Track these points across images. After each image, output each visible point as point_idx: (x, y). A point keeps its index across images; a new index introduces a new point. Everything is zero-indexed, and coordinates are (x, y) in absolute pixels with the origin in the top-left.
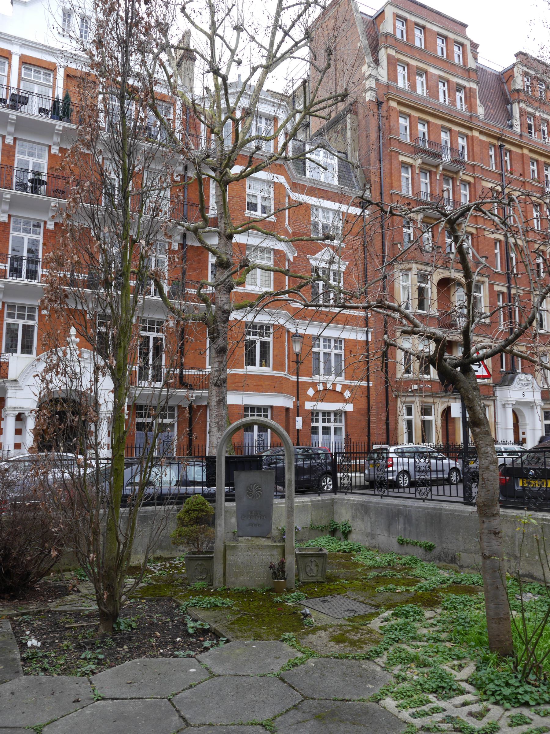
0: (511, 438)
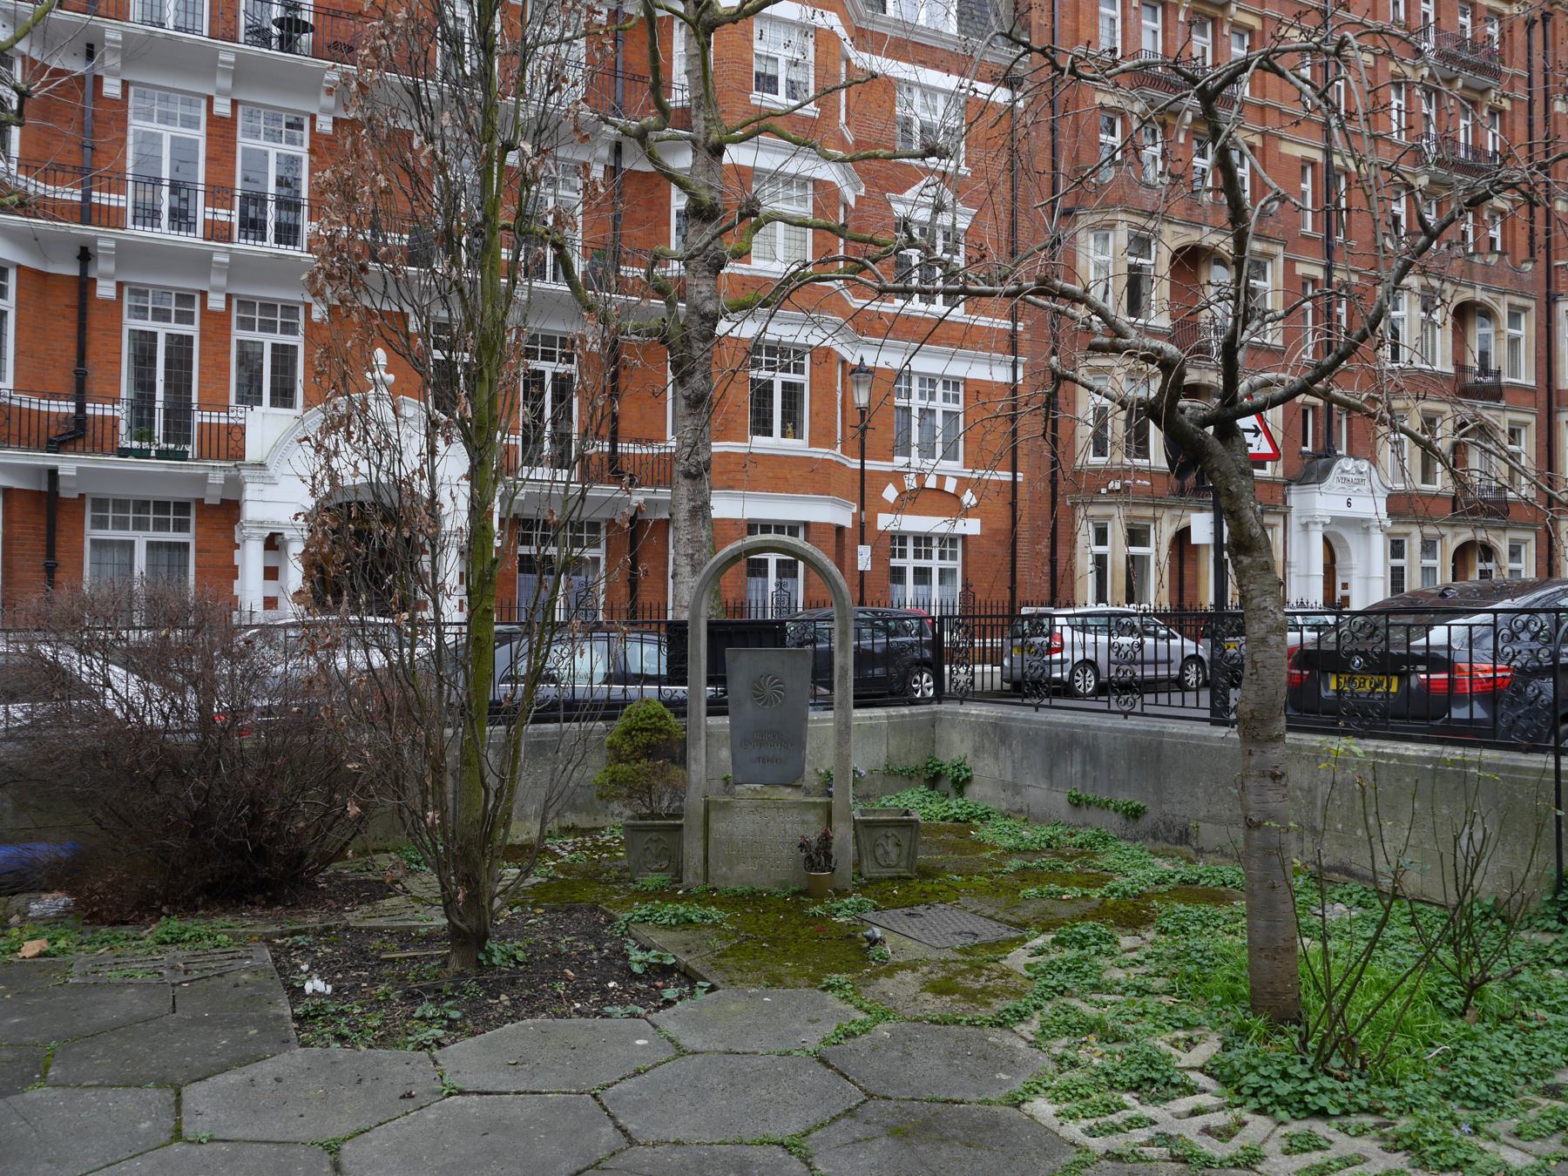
0: (1316, 596)
